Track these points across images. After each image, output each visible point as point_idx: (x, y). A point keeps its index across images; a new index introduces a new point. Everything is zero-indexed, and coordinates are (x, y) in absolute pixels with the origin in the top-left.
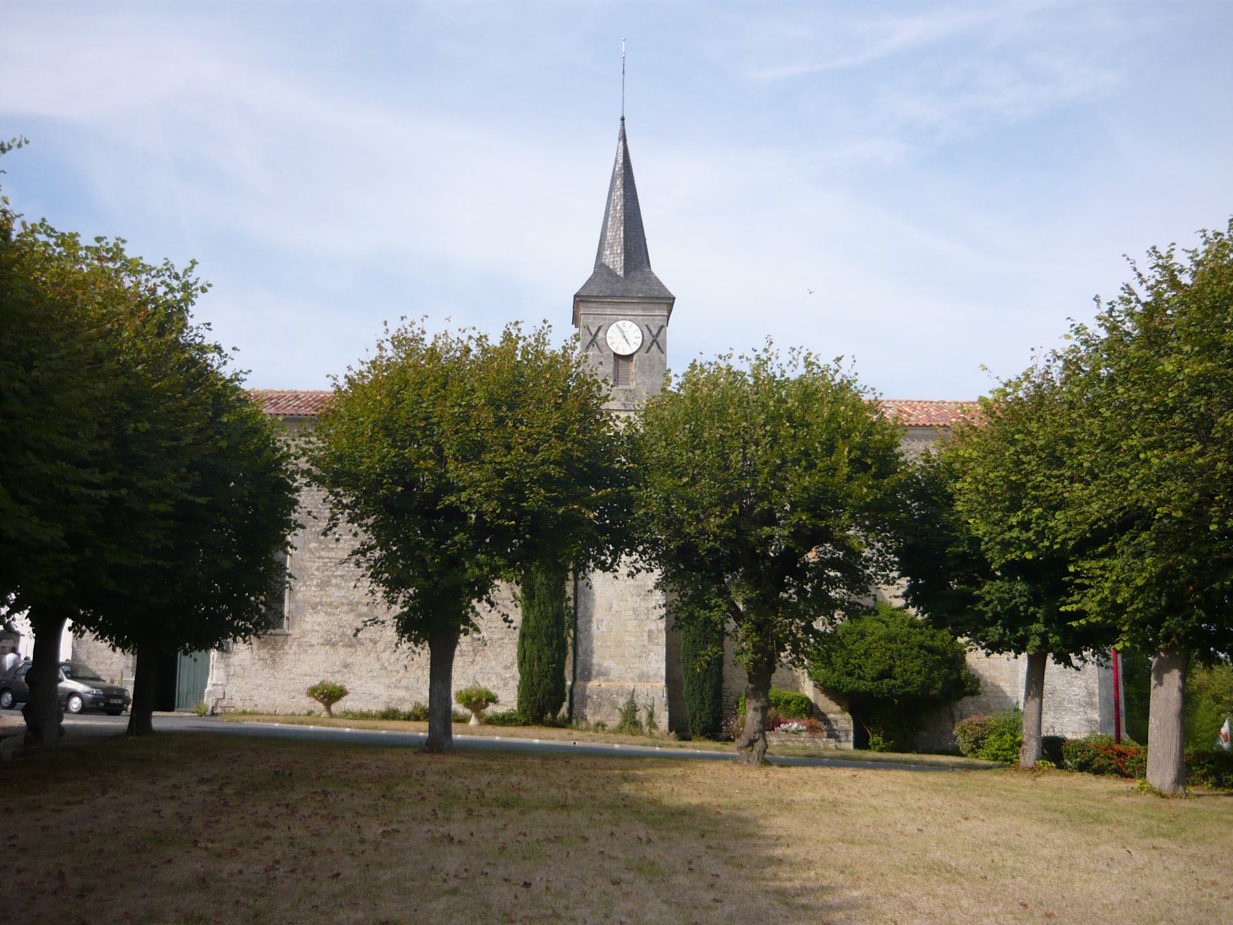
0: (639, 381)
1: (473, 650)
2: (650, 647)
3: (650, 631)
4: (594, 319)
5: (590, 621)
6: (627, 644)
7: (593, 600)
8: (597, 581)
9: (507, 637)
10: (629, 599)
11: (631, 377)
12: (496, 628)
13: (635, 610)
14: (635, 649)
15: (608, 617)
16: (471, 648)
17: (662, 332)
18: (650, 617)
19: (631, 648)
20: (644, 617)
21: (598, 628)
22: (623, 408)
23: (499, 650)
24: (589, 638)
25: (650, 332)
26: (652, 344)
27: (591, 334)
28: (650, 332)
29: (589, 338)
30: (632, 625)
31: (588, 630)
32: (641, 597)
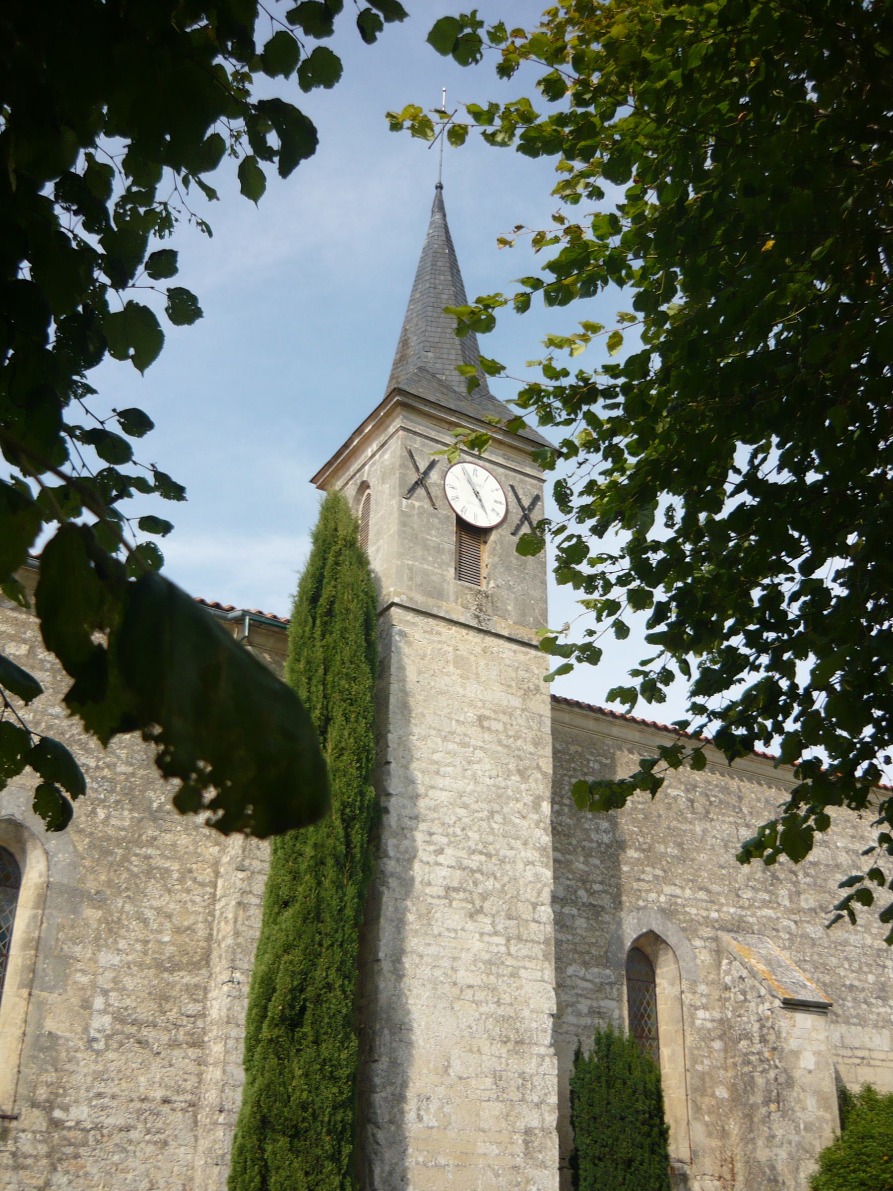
0: (500, 582)
1: (49, 1155)
2: (531, 1172)
3: (528, 1132)
4: (423, 445)
5: (401, 1098)
6: (481, 1162)
7: (410, 1044)
8: (418, 996)
9: (140, 1126)
10: (485, 1049)
11: (484, 572)
12: (113, 1097)
13: (497, 1077)
14: (497, 1175)
15: (441, 1090)
16: (43, 1149)
17: (537, 507)
18: (528, 1098)
19: (489, 1173)
20: (515, 1096)
21: (420, 1118)
22: (474, 623)
23: (116, 1158)
24: (399, 1142)
25: (519, 500)
26: (522, 523)
27: (417, 469)
28: (519, 500)
29: (414, 477)
30: (491, 1112)
31: (397, 1121)
32: (510, 1046)
